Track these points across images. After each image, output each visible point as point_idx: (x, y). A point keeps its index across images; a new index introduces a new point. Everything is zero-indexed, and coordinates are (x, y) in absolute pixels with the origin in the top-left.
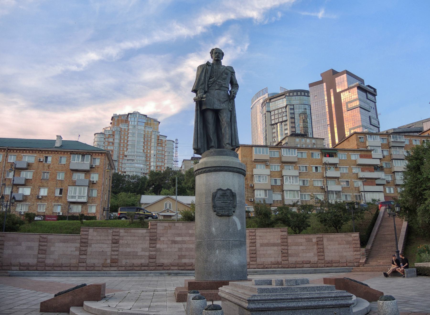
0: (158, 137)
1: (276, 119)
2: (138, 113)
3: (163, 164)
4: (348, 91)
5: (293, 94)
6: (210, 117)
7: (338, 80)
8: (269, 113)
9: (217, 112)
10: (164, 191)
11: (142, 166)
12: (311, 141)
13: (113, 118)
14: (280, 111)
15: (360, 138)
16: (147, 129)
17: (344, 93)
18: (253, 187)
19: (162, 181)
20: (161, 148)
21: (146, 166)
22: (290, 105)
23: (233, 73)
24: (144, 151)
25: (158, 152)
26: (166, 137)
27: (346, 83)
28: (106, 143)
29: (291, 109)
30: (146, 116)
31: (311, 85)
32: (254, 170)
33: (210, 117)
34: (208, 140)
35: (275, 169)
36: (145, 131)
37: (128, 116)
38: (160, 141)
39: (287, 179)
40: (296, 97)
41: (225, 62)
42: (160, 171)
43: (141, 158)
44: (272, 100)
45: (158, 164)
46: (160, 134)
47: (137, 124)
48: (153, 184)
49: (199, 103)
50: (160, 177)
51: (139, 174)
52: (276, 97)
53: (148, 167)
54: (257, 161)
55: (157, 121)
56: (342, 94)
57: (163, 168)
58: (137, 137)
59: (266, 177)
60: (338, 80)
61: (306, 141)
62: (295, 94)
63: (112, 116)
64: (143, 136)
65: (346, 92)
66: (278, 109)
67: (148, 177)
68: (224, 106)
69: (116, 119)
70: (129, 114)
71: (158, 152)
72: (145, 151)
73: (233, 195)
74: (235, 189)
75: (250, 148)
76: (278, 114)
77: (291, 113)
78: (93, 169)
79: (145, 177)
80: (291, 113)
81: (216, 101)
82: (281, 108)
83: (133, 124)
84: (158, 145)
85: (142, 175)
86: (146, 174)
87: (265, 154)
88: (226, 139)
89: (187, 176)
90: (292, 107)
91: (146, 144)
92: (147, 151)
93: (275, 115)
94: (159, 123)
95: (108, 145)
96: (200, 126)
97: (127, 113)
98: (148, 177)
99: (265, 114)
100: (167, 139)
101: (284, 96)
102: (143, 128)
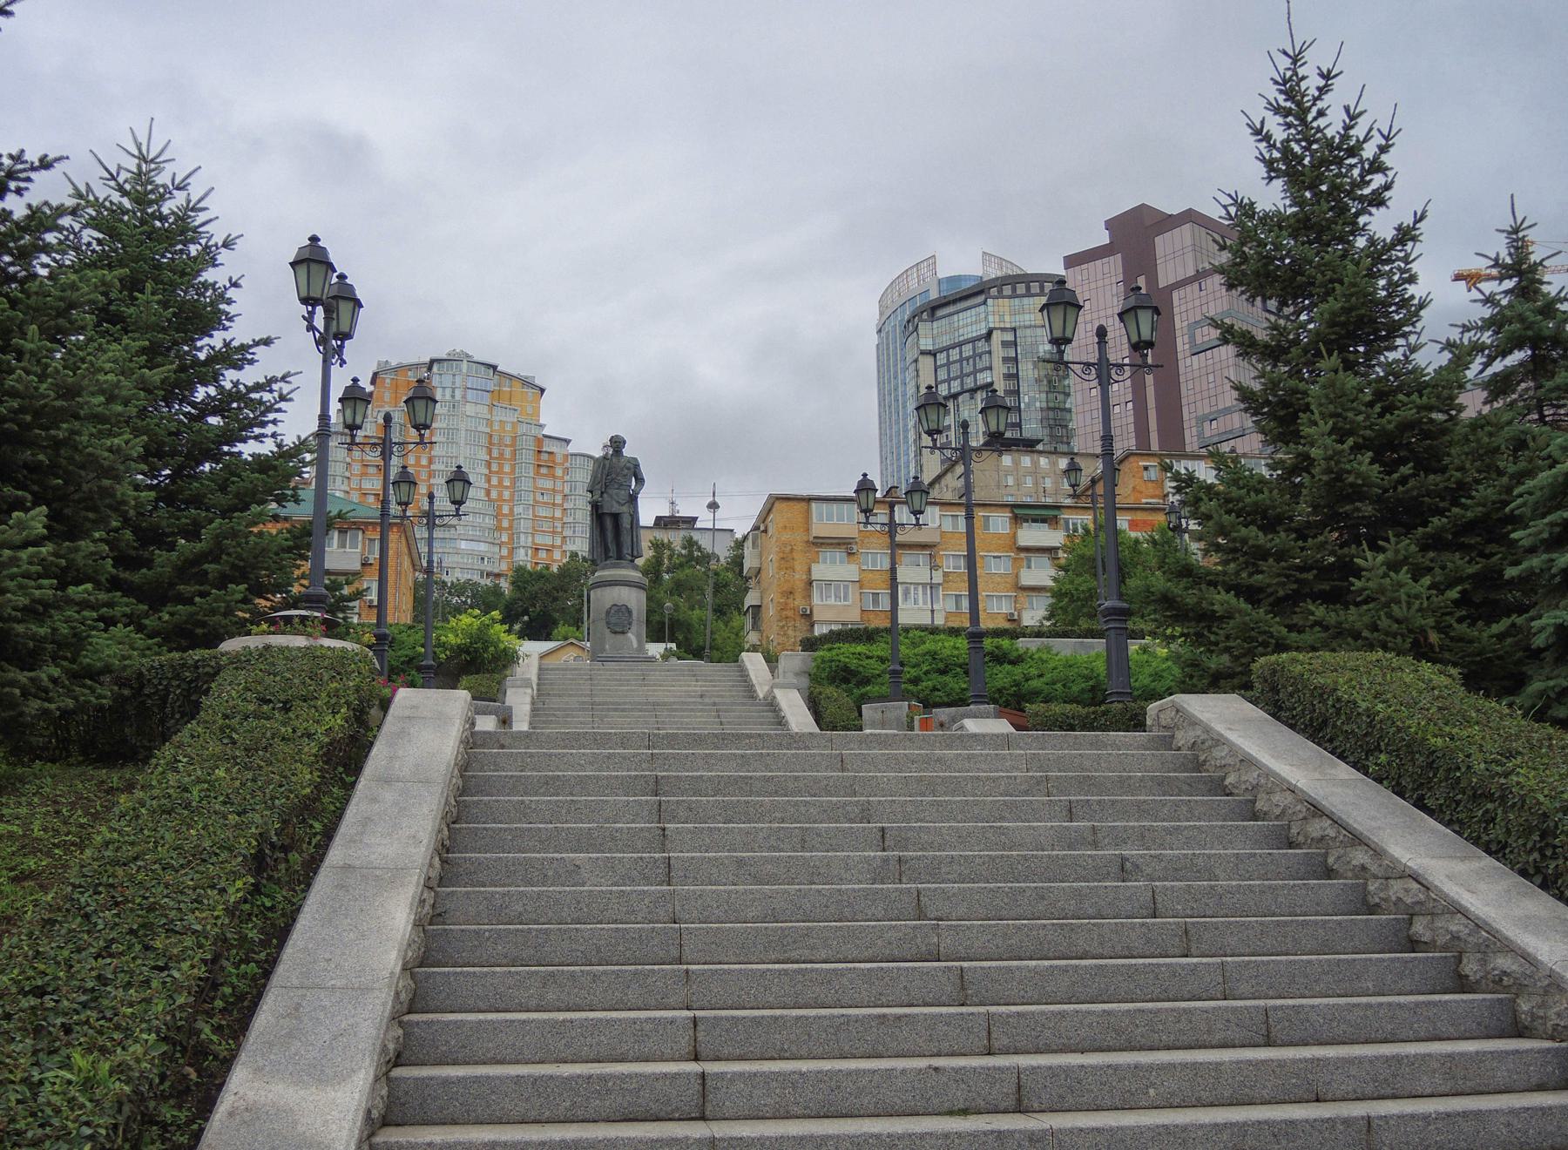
0: (539, 441)
1: (955, 379)
2: (468, 356)
3: (558, 542)
4: (1196, 285)
5: (1014, 290)
6: (609, 523)
7: (1163, 244)
8: (930, 359)
9: (616, 517)
10: (562, 629)
11: (483, 547)
12: (1055, 464)
13: (375, 375)
14: (967, 350)
15: (1146, 468)
16: (499, 415)
17: (1182, 292)
18: (810, 616)
19: (555, 599)
20: (548, 484)
21: (497, 549)
22: (1003, 329)
23: (637, 466)
24: (488, 493)
25: (539, 498)
26: (567, 442)
27: (1189, 258)
28: (357, 468)
29: (1005, 344)
30: (494, 368)
31: (1072, 261)
32: (814, 567)
33: (609, 523)
34: (606, 550)
35: (875, 563)
36: (490, 423)
37: (430, 369)
38: (545, 457)
39: (907, 592)
40: (1026, 300)
41: (627, 452)
42: (547, 568)
43: (479, 520)
44: (940, 313)
45: (539, 540)
46: (546, 432)
47: (464, 397)
48: (526, 612)
49: (596, 507)
50: (548, 586)
51: (476, 578)
52: (954, 302)
53: (505, 552)
54: (821, 543)
55: (534, 386)
56: (1175, 295)
57: (557, 555)
58: (462, 442)
59: (846, 587)
60: (1163, 244)
61: (1035, 464)
62: (1021, 289)
63: (374, 368)
64: (484, 441)
65: (1188, 288)
66: (960, 345)
67: (505, 585)
68: (625, 509)
69: (388, 379)
70: (432, 362)
71: (539, 498)
72: (494, 495)
73: (630, 612)
74: (633, 605)
75: (803, 504)
76: (961, 360)
77: (1006, 360)
78: (368, 569)
79: (497, 586)
80: (1006, 360)
81: (611, 506)
82: (973, 341)
83: (448, 397)
84: (538, 473)
85: (488, 582)
86: (498, 576)
87: (845, 521)
88: (626, 550)
89: (1384, 396)
90: (1009, 337)
91: (495, 467)
92: (500, 494)
93: (948, 364)
94: (542, 391)
95: (364, 474)
96: (597, 532)
97: (427, 360)
98: (505, 585)
99: (916, 361)
100: (571, 449)
101: (981, 299)
102: (483, 411)
